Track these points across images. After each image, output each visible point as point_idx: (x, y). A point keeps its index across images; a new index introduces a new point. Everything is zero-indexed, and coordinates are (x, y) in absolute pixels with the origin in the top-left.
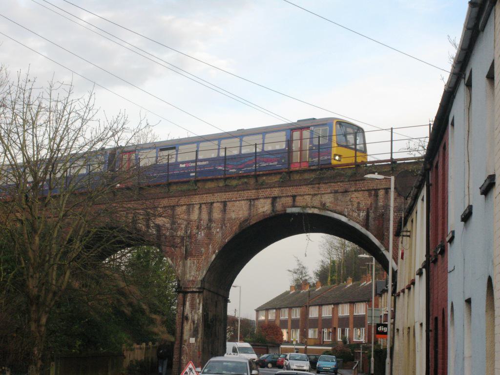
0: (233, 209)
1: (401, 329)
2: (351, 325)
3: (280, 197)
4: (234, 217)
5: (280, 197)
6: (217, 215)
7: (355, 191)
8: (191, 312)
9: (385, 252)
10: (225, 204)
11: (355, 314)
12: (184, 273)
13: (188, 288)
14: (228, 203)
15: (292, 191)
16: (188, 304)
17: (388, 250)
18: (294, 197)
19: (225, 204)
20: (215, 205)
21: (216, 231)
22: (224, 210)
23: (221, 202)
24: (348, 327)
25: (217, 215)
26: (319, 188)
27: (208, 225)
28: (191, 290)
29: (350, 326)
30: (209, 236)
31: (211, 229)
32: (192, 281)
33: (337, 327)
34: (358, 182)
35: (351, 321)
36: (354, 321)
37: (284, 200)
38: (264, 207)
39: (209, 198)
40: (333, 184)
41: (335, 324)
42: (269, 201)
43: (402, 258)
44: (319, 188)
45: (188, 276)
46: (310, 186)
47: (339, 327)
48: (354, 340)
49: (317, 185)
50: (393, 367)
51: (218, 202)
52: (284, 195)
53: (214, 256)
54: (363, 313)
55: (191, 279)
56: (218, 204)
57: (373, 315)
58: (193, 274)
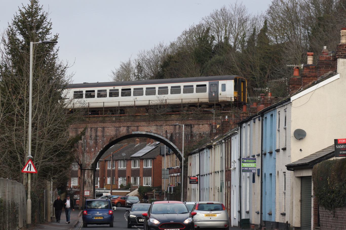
0: (108, 131)
1: (190, 189)
2: (141, 175)
3: (131, 127)
4: (108, 135)
5: (131, 127)
6: (99, 134)
7: (166, 125)
8: (88, 179)
9: (180, 153)
10: (103, 128)
11: (144, 167)
12: (84, 160)
13: (86, 167)
14: (105, 128)
15: (137, 124)
16: (86, 175)
17: (181, 151)
18: (138, 127)
19: (103, 128)
20: (98, 128)
21: (100, 141)
22: (103, 131)
23: (102, 127)
24: (139, 176)
25: (99, 134)
26: (149, 123)
27: (95, 138)
28: (87, 168)
29: (140, 176)
30: (96, 143)
31: (97, 140)
32: (88, 164)
33: (130, 176)
34: (167, 122)
35: (141, 172)
36: (143, 172)
37: (133, 128)
38: (123, 131)
39: (95, 126)
40: (155, 122)
41: (128, 174)
42: (125, 128)
43: (190, 165)
44: (149, 123)
45: (85, 162)
46: (145, 122)
47: (132, 176)
48: (144, 185)
49: (149, 122)
50: (286, 180)
51: (100, 127)
52: (133, 126)
53: (99, 153)
54: (151, 166)
55: (87, 163)
56: (100, 129)
57: (165, 174)
58: (88, 161)
